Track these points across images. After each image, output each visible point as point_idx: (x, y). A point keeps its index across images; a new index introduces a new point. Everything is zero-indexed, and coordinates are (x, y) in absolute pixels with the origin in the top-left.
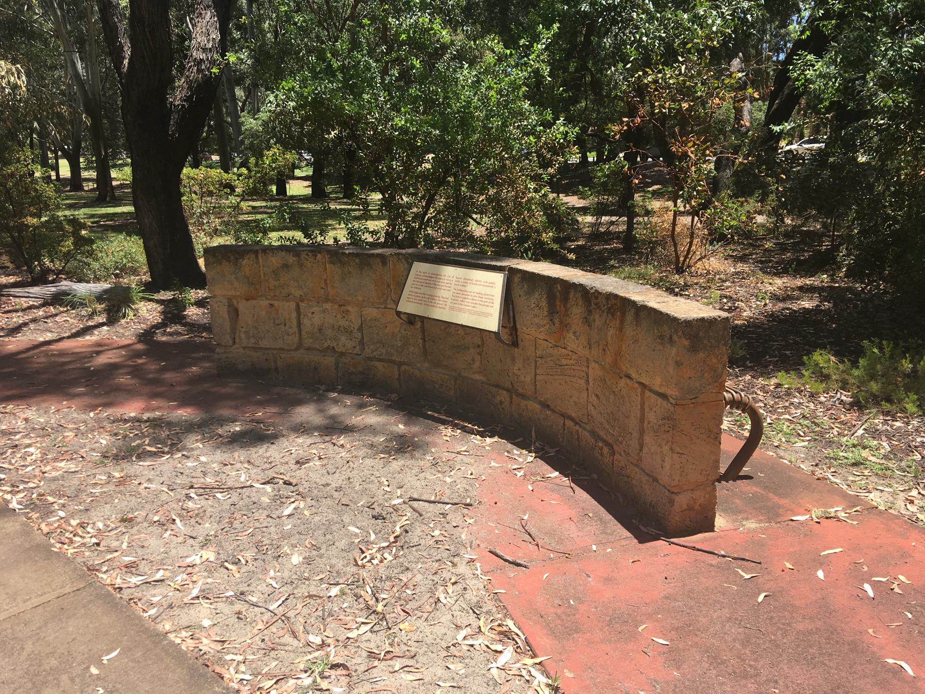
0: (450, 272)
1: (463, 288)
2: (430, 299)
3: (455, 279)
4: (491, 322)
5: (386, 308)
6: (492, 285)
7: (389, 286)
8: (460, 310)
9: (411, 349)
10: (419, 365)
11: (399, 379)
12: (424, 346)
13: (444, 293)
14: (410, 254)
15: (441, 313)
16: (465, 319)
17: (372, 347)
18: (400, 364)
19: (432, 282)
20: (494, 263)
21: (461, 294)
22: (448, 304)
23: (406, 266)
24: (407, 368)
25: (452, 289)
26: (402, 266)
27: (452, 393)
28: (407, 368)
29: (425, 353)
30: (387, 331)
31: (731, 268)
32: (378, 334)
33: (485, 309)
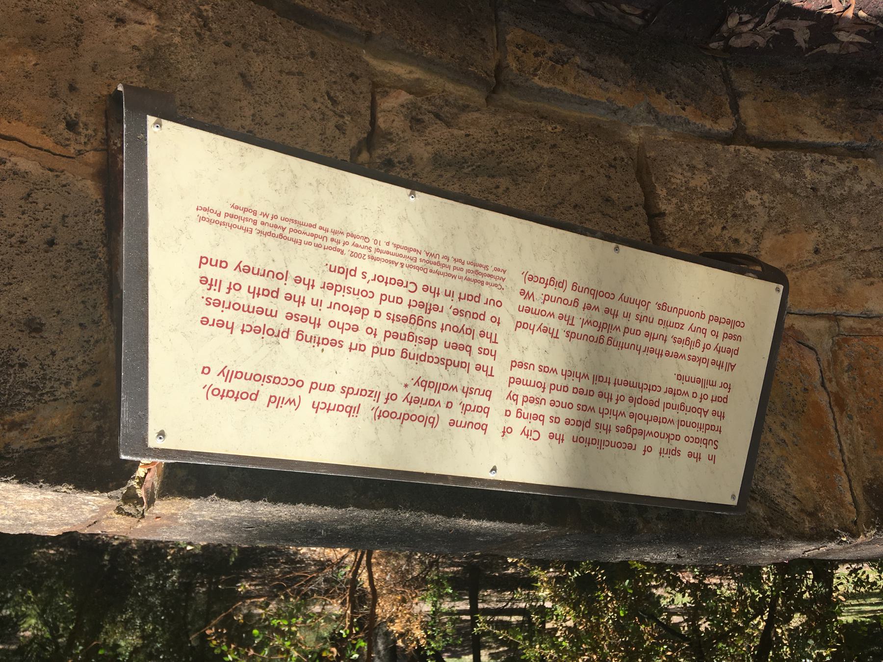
0: (512, 452)
1: (434, 372)
2: (605, 323)
3: (496, 421)
4: (191, 176)
5: (834, 318)
6: (232, 386)
7: (838, 402)
8: (433, 262)
9: (700, 181)
10: (663, 134)
11: (735, 97)
12: (649, 194)
13: (526, 349)
14: (762, 537)
15: (523, 251)
16: (386, 218)
17: (859, 188)
18: (738, 136)
19: (597, 405)
20: (284, 512)
21: (440, 334)
22: (512, 302)
23: (775, 488)
24: (708, 124)
25: (502, 373)
26: (795, 483)
27: (514, 34)
28: (708, 124)
29: (643, 171)
30: (813, 238)
31: (554, 531)
32: (847, 227)
33: (238, 247)
